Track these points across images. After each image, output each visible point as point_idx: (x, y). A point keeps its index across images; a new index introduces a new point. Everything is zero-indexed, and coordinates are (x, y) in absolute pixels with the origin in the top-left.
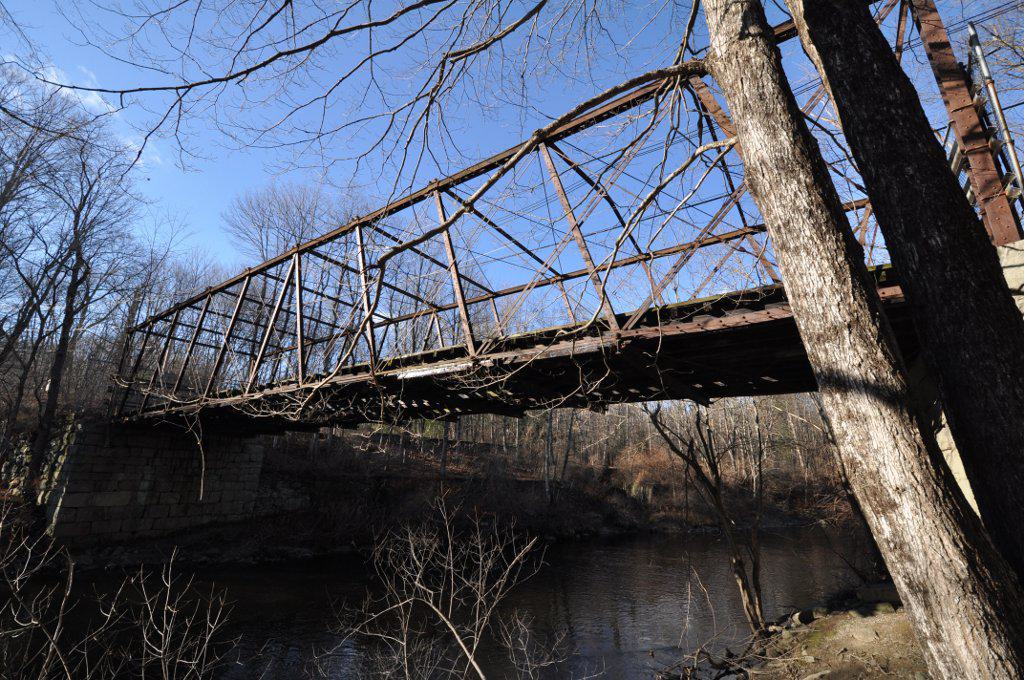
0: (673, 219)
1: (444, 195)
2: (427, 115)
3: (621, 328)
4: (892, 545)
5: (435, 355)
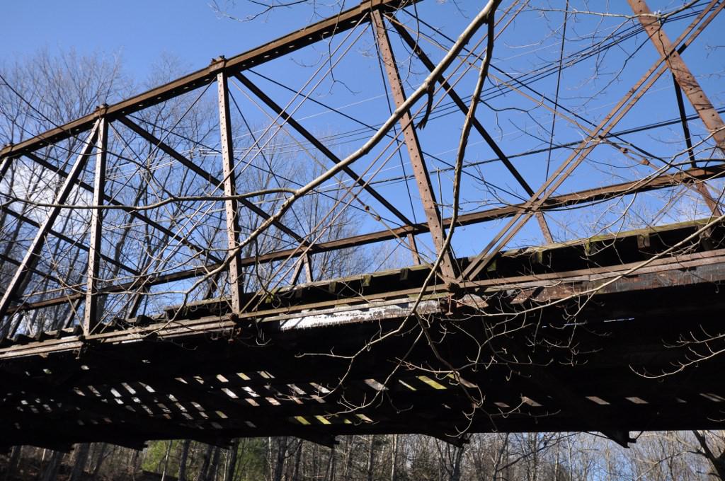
1: (233, 81)
3: (457, 276)
5: (367, 283)
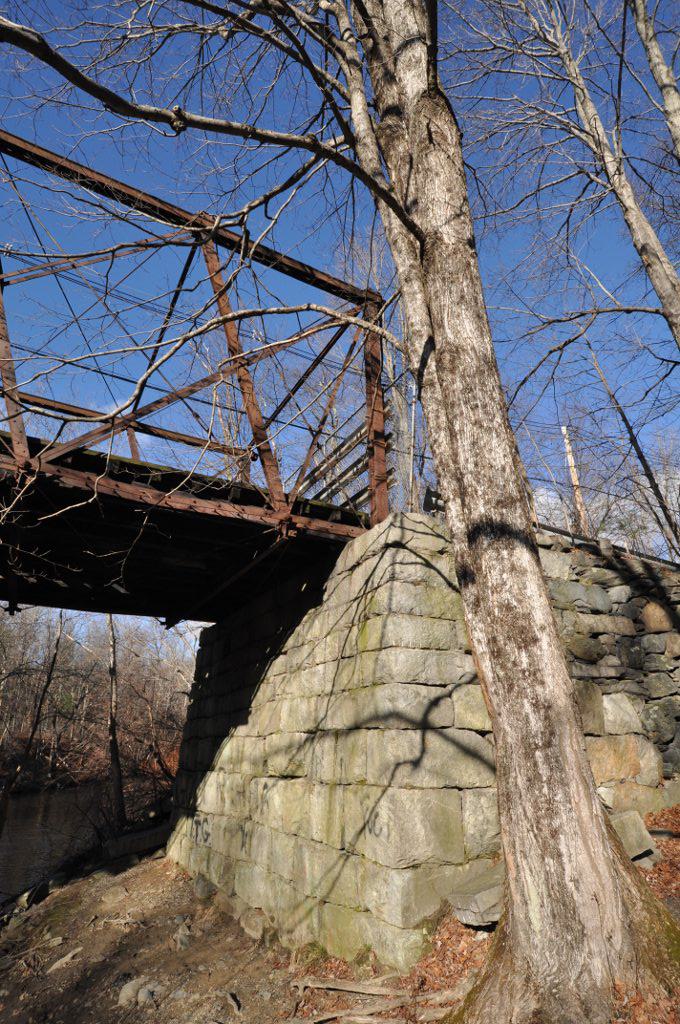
0: (141, 353)
2: (289, 51)
4: (527, 673)
